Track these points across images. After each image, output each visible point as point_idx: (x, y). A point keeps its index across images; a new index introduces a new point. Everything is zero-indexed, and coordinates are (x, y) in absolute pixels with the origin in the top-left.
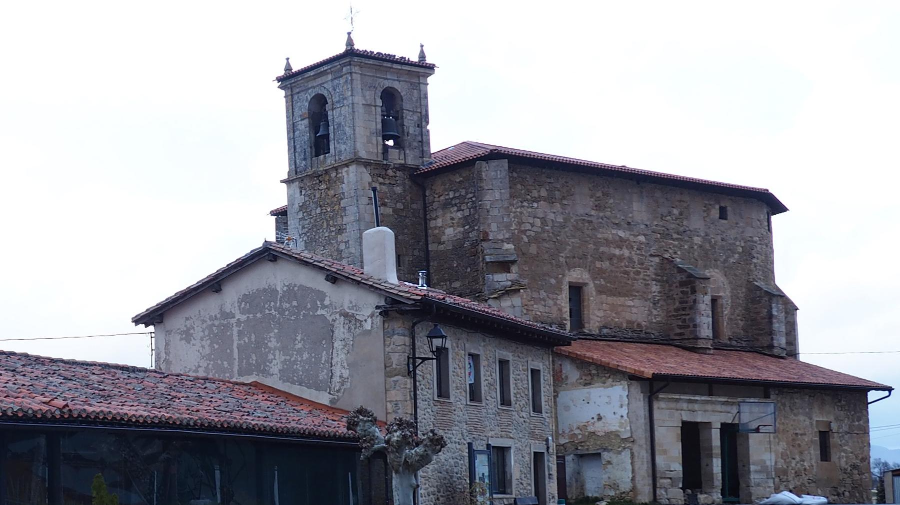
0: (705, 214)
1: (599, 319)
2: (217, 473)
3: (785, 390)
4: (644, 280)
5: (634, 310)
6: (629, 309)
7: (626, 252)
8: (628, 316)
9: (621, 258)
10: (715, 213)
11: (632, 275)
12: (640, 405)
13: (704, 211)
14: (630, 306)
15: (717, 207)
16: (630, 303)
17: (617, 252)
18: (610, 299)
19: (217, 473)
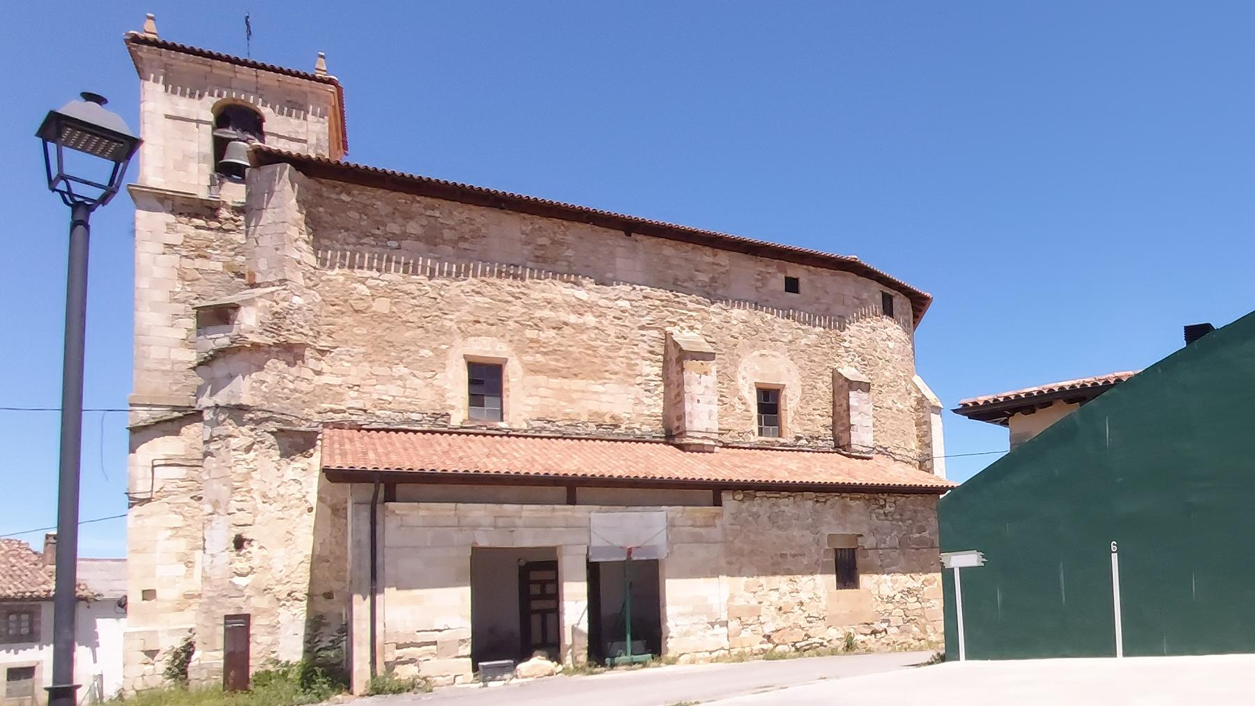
0: (759, 284)
1: (530, 409)
2: (1115, 557)
3: (758, 494)
4: (627, 358)
5: (604, 398)
6: (595, 396)
7: (590, 319)
8: (593, 406)
9: (581, 328)
10: (778, 283)
11: (602, 351)
12: (356, 524)
13: (758, 280)
14: (595, 393)
15: (782, 276)
16: (600, 388)
17: (573, 319)
18: (556, 382)
19: (1115, 557)
